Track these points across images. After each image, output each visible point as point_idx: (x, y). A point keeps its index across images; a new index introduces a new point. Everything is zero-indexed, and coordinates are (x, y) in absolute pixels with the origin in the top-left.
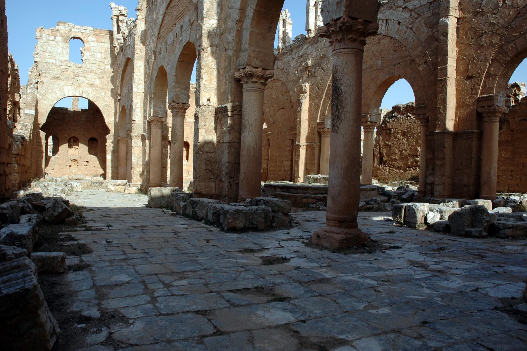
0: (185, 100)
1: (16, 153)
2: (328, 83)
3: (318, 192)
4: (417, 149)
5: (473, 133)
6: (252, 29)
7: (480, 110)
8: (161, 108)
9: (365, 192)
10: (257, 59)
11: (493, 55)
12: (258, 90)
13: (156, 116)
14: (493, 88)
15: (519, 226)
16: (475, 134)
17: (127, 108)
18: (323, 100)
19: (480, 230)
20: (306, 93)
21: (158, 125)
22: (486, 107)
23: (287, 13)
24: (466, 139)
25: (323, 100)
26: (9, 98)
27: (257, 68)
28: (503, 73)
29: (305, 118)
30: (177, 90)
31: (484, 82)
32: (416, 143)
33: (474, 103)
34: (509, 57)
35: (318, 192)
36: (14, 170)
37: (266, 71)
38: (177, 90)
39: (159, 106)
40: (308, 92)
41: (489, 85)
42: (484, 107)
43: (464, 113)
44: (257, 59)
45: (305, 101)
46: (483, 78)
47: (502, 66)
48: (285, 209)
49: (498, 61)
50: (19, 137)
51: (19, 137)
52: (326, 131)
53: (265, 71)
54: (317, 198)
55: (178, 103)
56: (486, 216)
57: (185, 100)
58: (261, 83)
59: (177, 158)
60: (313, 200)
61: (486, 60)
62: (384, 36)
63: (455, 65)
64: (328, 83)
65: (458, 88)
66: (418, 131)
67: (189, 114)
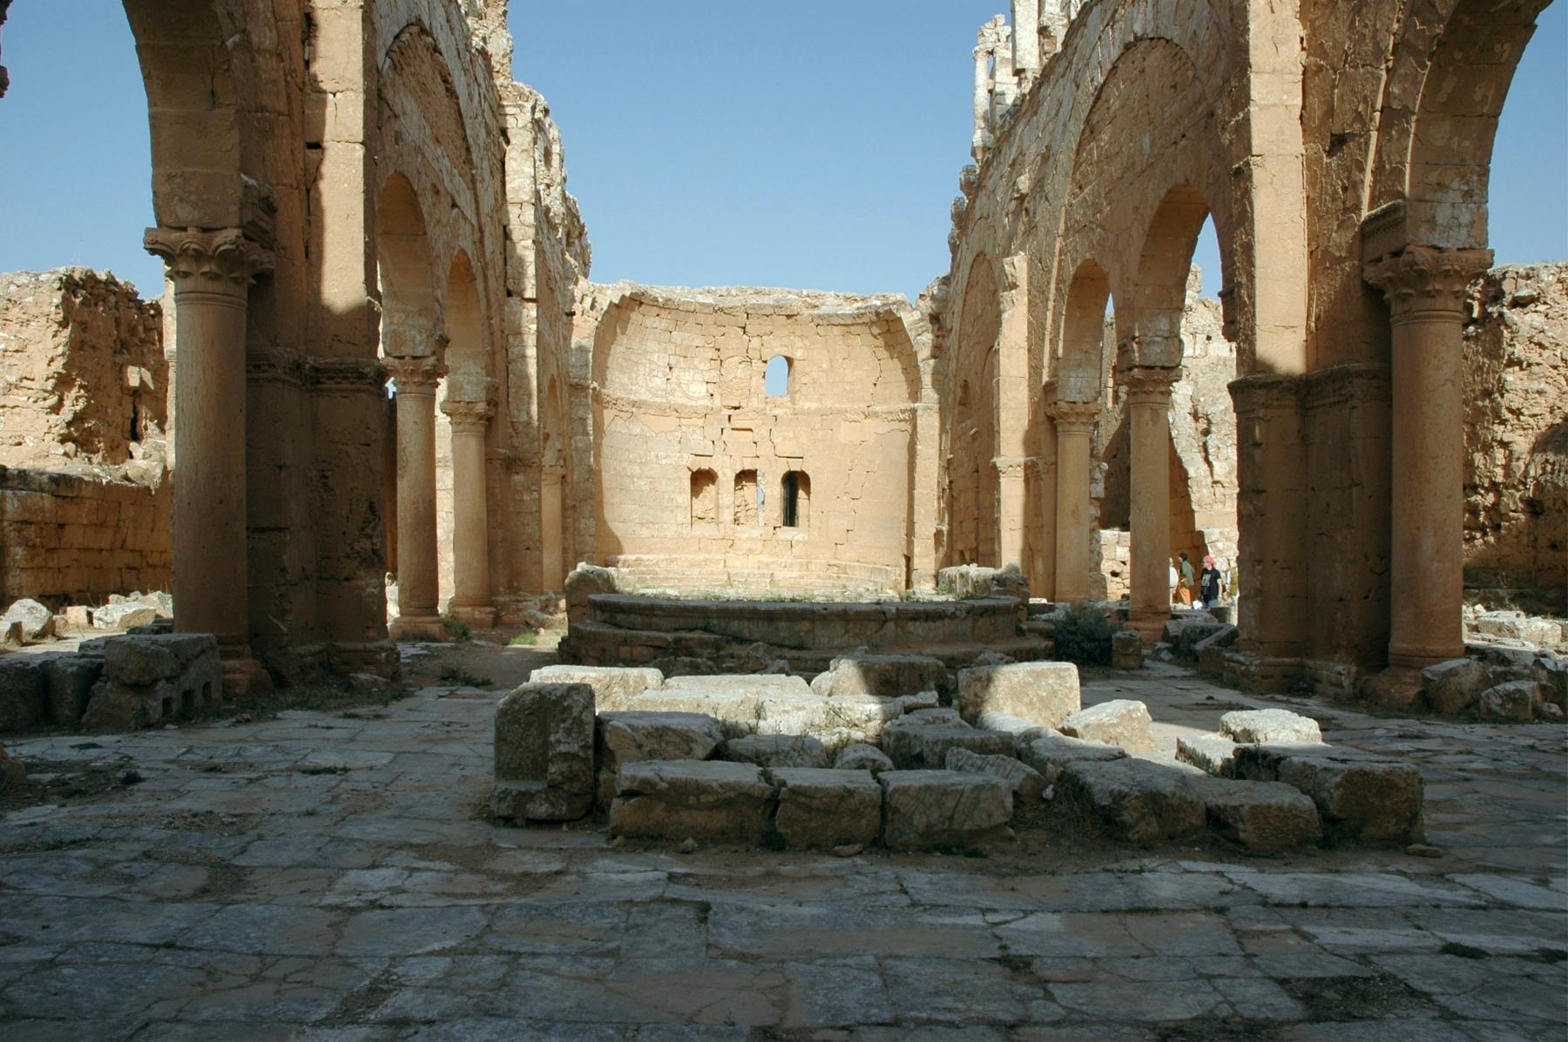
0: (422, 347)
1: (16, 517)
2: (1058, 245)
3: (682, 622)
4: (1473, 460)
5: (1347, 375)
6: (155, 109)
7: (1372, 274)
8: (469, 374)
9: (873, 626)
10: (181, 200)
11: (1396, 26)
12: (210, 299)
13: (458, 399)
14: (1401, 173)
15: (701, 789)
16: (1357, 381)
17: (975, 388)
18: (1051, 304)
19: (520, 793)
20: (1014, 286)
21: (467, 426)
22: (1387, 260)
23: (999, 29)
24: (1335, 403)
25: (1051, 304)
26: (75, 380)
27: (184, 229)
28: (1442, 97)
29: (1013, 373)
30: (395, 320)
31: (1379, 152)
32: (1469, 438)
33: (1351, 245)
34: (1440, 19)
35: (682, 622)
36: (15, 561)
37: (215, 233)
38: (395, 320)
39: (462, 370)
40: (1023, 284)
41: (1390, 163)
42: (1380, 260)
43: (1329, 297)
44: (181, 200)
45: (1013, 315)
46: (1374, 135)
47: (1424, 66)
48: (121, 669)
49: (1412, 50)
50: (45, 479)
51: (45, 479)
52: (1066, 414)
53: (207, 235)
54: (657, 643)
55: (402, 358)
56: (568, 732)
57: (422, 347)
58: (204, 274)
59: (409, 520)
60: (645, 651)
61: (1379, 53)
62: (1152, 39)
63: (1299, 102)
64: (1058, 245)
65: (1312, 196)
66: (1473, 391)
67: (805, 387)
